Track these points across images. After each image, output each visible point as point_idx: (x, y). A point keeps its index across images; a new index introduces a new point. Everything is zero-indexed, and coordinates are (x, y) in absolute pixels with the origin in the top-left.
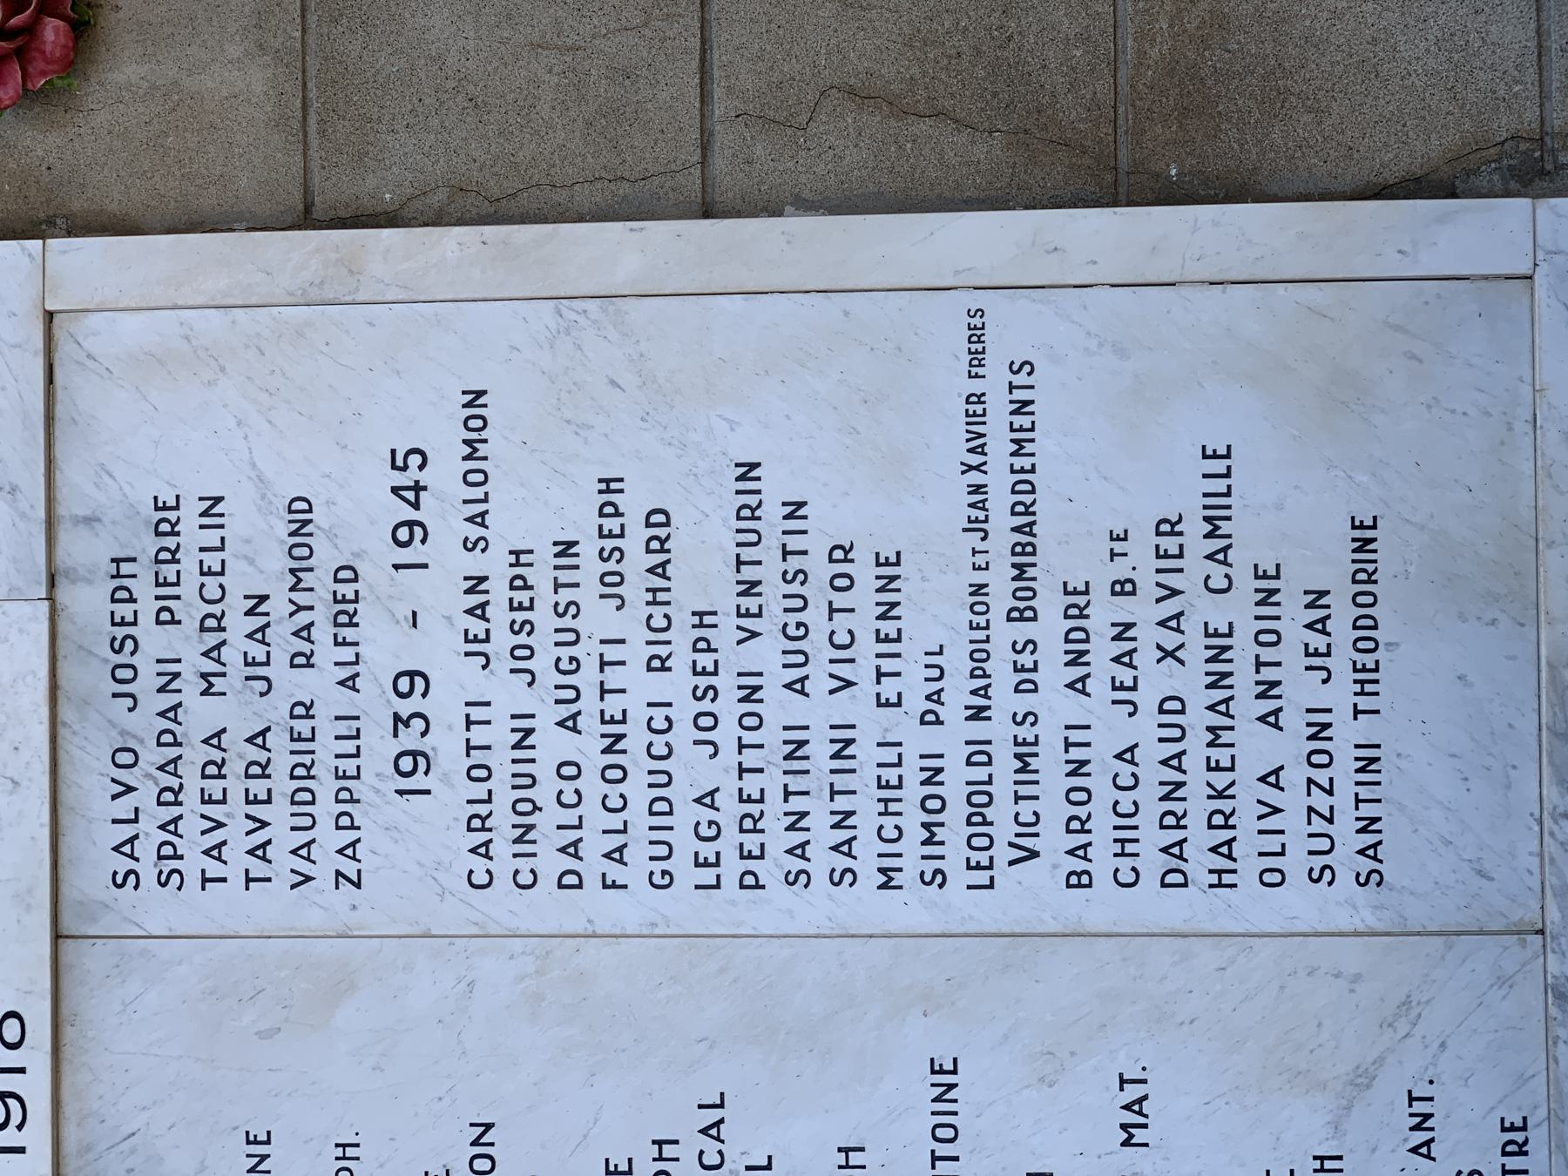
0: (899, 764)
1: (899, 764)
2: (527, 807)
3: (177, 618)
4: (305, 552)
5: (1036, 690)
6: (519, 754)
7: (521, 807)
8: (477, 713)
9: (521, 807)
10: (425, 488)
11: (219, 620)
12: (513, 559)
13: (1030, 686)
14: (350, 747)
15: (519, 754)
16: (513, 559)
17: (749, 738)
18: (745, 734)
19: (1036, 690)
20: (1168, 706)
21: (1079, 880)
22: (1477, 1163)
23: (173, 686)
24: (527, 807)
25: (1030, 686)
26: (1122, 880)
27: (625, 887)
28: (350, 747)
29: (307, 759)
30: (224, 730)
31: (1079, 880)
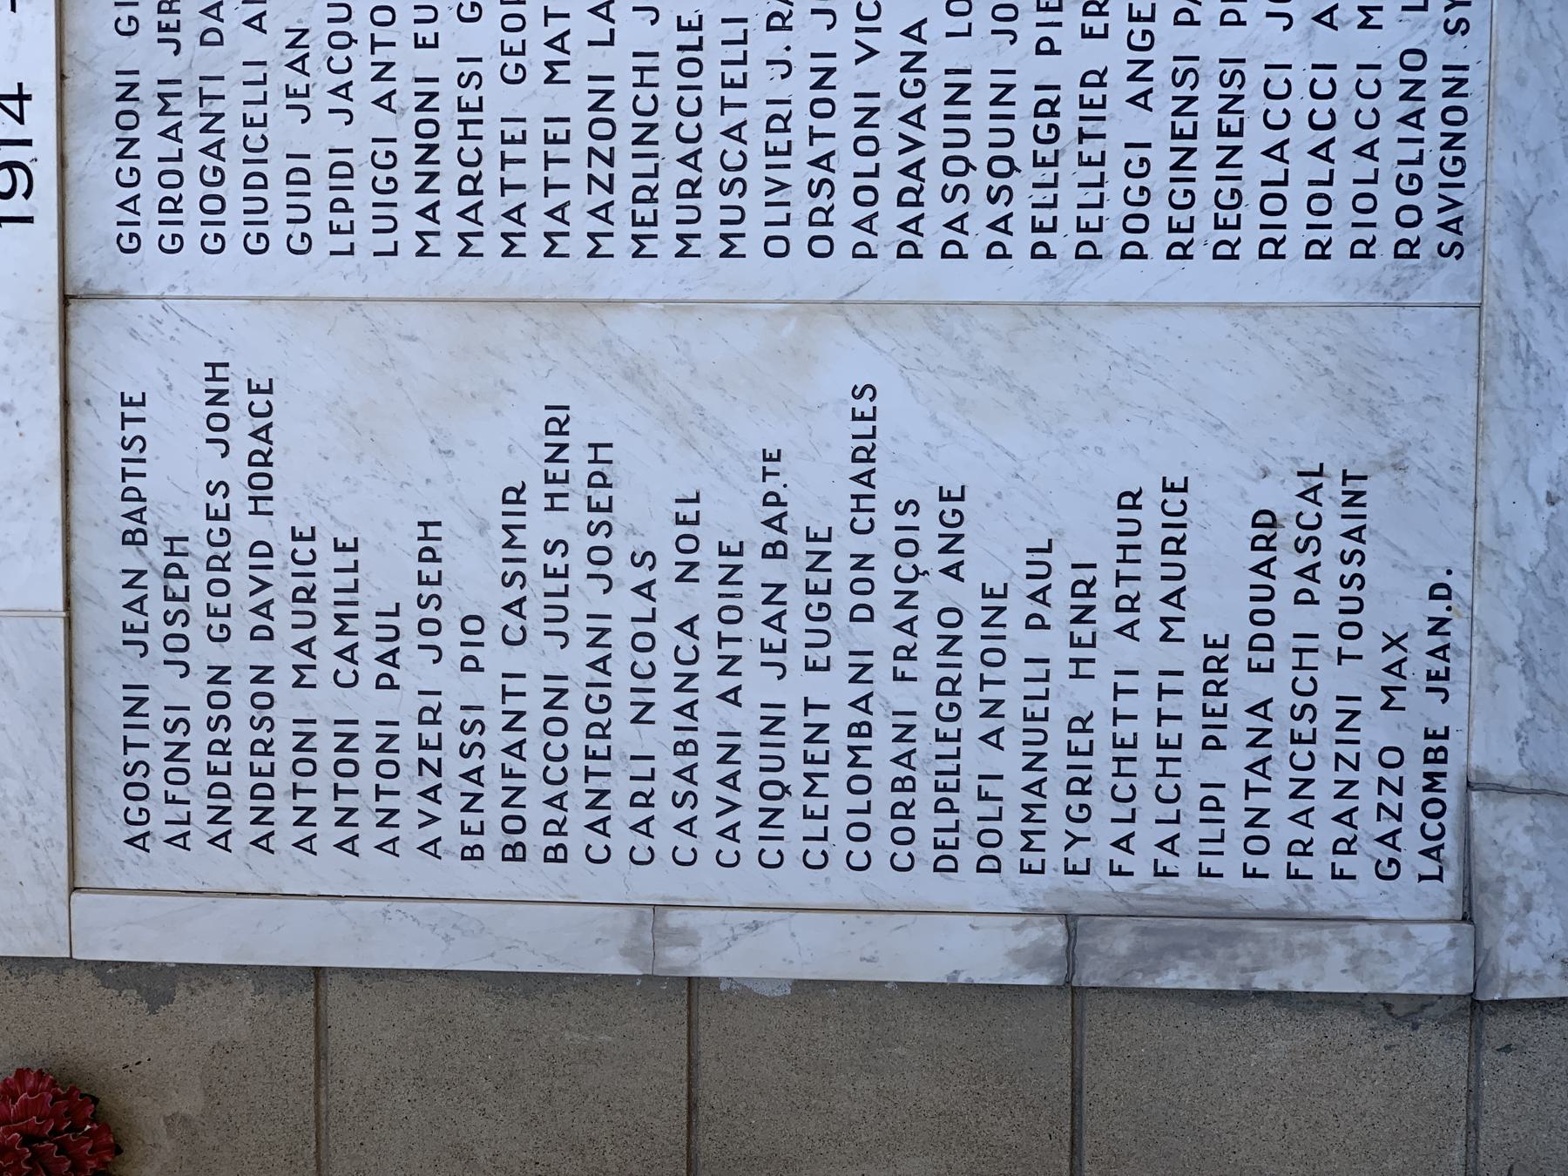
0: (744, 62)
1: (744, 62)
2: (776, 790)
3: (608, 482)
4: (264, 481)
5: (271, 638)
6: (647, 697)
7: (768, 790)
8: (513, 685)
9: (768, 790)
10: (29, 97)
11: (785, 121)
12: (208, 372)
13: (266, 633)
14: (1038, 689)
15: (647, 697)
16: (208, 372)
17: (345, 784)
18: (340, 780)
19: (271, 638)
20: (257, 550)
21: (774, 551)
22: (278, 908)
23: (864, 677)
24: (776, 790)
25: (266, 633)
26: (1271, 122)
27: (1353, 877)
28: (1038, 689)
29: (1084, 774)
30: (1270, 700)
31: (774, 551)
